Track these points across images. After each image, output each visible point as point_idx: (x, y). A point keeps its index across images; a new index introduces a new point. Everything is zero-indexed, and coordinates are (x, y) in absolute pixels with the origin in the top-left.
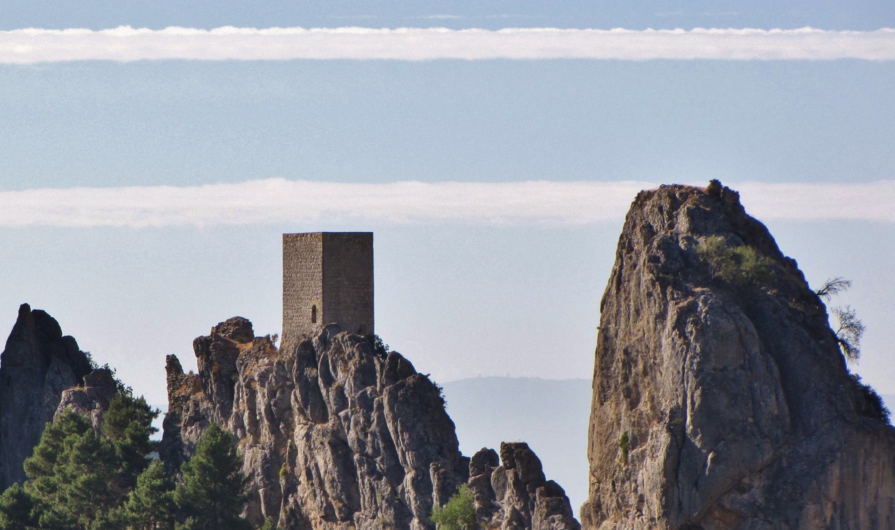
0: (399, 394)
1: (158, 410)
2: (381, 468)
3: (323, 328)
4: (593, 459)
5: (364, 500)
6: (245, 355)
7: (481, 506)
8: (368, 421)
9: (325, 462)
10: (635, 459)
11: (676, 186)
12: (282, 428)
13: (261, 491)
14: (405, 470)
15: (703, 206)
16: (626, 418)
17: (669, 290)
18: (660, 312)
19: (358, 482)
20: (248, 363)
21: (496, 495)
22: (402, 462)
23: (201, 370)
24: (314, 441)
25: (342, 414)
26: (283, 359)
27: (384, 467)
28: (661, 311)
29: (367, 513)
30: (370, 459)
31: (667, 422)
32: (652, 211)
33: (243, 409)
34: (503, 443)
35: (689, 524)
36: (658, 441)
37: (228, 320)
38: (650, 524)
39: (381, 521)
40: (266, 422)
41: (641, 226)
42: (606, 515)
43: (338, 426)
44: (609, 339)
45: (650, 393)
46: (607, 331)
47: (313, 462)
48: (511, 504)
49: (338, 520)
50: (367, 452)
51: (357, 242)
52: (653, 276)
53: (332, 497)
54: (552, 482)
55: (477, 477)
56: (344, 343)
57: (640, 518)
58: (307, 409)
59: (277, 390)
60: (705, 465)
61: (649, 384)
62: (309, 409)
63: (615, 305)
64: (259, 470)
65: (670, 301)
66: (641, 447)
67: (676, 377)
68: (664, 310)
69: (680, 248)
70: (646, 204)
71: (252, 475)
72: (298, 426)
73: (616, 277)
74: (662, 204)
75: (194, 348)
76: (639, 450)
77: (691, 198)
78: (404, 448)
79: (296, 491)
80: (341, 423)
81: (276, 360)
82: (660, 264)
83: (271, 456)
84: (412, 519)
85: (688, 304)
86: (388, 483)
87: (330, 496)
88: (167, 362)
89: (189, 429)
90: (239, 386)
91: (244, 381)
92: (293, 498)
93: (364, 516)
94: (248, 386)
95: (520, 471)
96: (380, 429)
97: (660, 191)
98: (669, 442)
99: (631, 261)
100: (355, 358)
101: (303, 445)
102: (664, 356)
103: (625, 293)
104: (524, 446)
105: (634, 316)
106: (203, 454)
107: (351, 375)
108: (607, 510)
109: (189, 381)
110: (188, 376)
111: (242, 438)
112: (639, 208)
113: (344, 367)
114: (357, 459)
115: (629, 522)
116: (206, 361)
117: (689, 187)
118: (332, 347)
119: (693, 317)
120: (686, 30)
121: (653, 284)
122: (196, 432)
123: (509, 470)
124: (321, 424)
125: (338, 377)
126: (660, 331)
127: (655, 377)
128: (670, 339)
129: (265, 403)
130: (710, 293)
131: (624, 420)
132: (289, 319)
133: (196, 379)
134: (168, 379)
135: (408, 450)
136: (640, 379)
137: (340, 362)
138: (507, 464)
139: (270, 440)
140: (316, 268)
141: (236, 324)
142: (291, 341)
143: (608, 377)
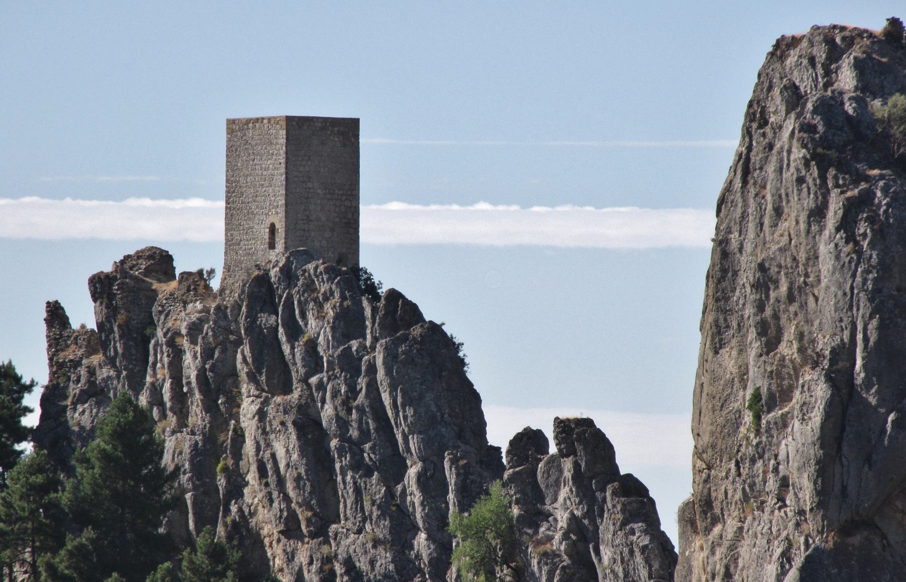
0: (400, 350)
1: (33, 381)
2: (371, 459)
3: (286, 255)
4: (701, 434)
5: (345, 507)
6: (166, 299)
7: (522, 512)
8: (353, 392)
9: (287, 451)
10: (771, 426)
11: (835, 27)
12: (221, 403)
13: (188, 496)
14: (408, 461)
15: (877, 55)
16: (756, 369)
17: (832, 172)
18: (817, 206)
19: (336, 480)
20: (170, 311)
21: (546, 495)
22: (403, 450)
23: (100, 320)
24: (270, 422)
25: (314, 380)
26: (225, 303)
27: (375, 458)
28: (817, 204)
29: (349, 524)
30: (354, 447)
31: (826, 367)
32: (798, 65)
33: (162, 377)
34: (557, 419)
35: (857, 519)
36: (811, 396)
37: (138, 252)
38: (797, 520)
39: (369, 537)
40: (197, 396)
41: (782, 86)
42: (720, 516)
43: (307, 398)
44: (730, 256)
45: (797, 327)
46: (727, 243)
47: (269, 452)
48: (568, 508)
49: (306, 537)
50: (351, 436)
51: (336, 132)
52: (807, 153)
53: (297, 503)
54: (629, 476)
55: (517, 469)
56: (317, 276)
57: (782, 511)
58: (261, 374)
59: (215, 348)
60: (884, 431)
61: (796, 314)
62: (264, 374)
63: (740, 205)
64: (187, 466)
65: (832, 189)
66: (781, 409)
67: (841, 301)
68: (822, 202)
69: (846, 113)
70: (789, 55)
71: (177, 469)
72: (247, 399)
73: (741, 162)
74: (814, 54)
75: (90, 289)
76: (777, 413)
77: (859, 44)
78: (406, 430)
79: (242, 495)
80: (311, 394)
81: (213, 305)
82: (817, 136)
83: (204, 445)
84: (417, 534)
85: (859, 193)
86: (382, 482)
87: (294, 501)
88: (48, 312)
89: (80, 408)
90: (157, 344)
91: (165, 335)
92: (236, 506)
93: (345, 530)
94: (171, 343)
95: (582, 460)
96: (370, 402)
97: (812, 34)
98: (828, 396)
99: (764, 139)
100: (334, 298)
101: (254, 428)
102: (822, 270)
103: (755, 187)
104: (588, 423)
105: (771, 217)
106: (107, 438)
107: (329, 323)
108: (722, 509)
109: (80, 339)
110: (78, 332)
111: (160, 420)
112: (778, 61)
113: (318, 311)
114: (335, 446)
115: (765, 518)
116: (107, 307)
117: (855, 29)
118: (300, 283)
119: (867, 213)
120: (523, 208)
121: (807, 164)
122: (91, 412)
123: (565, 459)
124: (282, 396)
125: (309, 326)
126: (816, 235)
127: (806, 303)
128: (832, 245)
129: (196, 367)
130: (893, 177)
131: (754, 371)
132: (234, 244)
133: (90, 336)
134: (48, 336)
135: (412, 432)
136: (782, 307)
137: (311, 304)
138: (562, 449)
139: (204, 421)
140: (276, 169)
141: (150, 257)
142: (237, 277)
143: (727, 311)
